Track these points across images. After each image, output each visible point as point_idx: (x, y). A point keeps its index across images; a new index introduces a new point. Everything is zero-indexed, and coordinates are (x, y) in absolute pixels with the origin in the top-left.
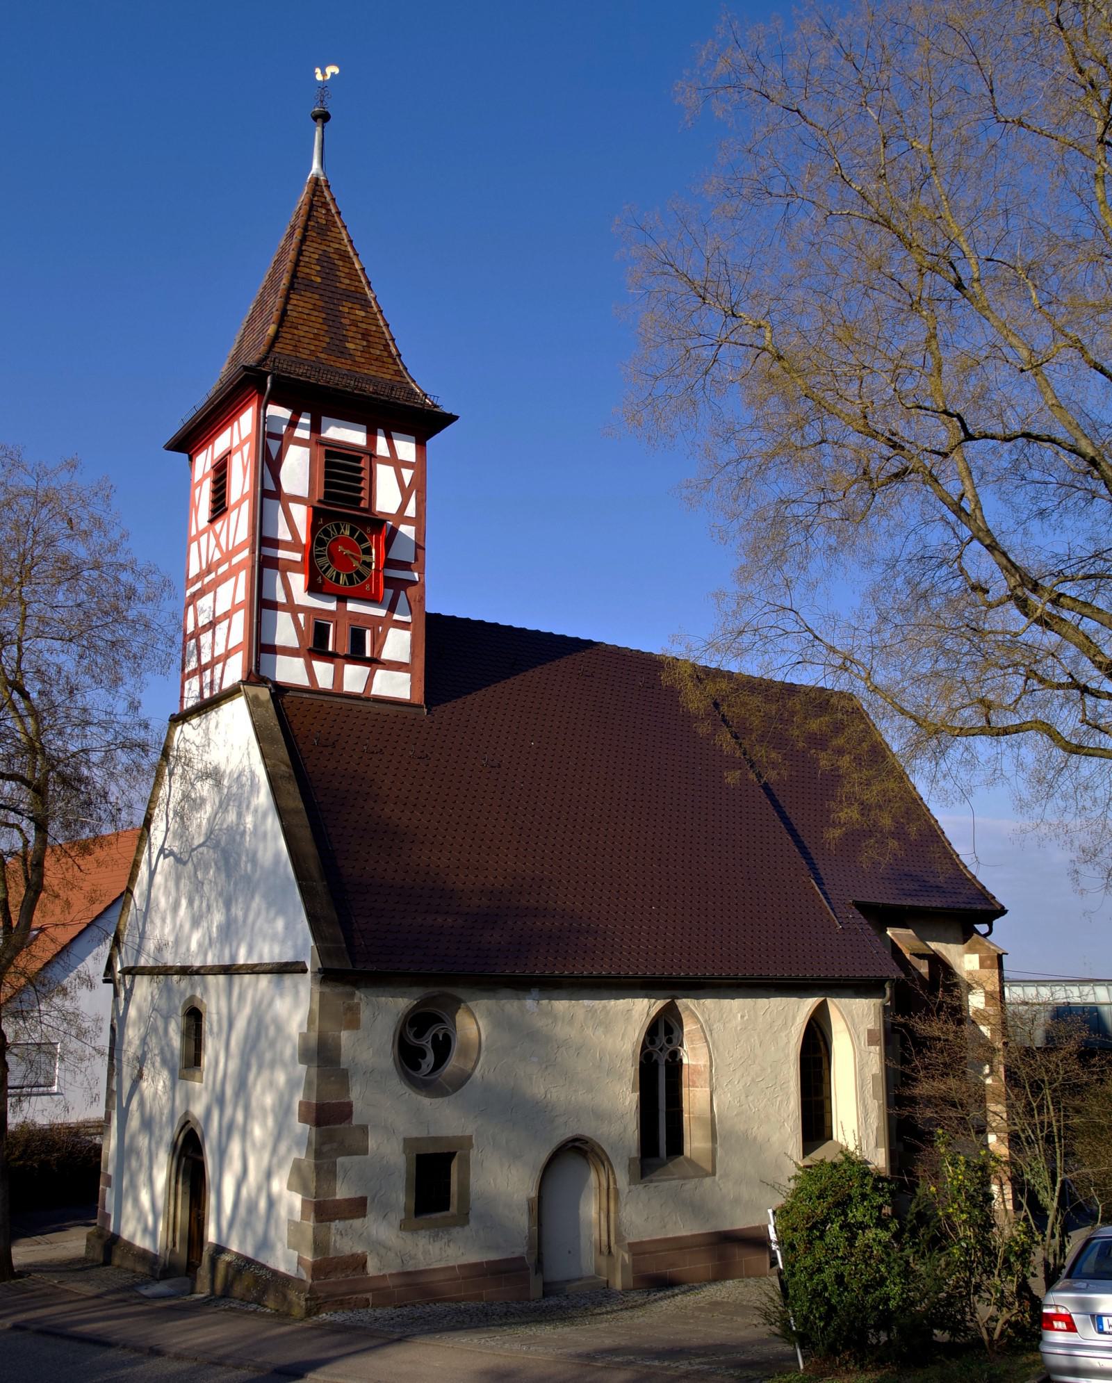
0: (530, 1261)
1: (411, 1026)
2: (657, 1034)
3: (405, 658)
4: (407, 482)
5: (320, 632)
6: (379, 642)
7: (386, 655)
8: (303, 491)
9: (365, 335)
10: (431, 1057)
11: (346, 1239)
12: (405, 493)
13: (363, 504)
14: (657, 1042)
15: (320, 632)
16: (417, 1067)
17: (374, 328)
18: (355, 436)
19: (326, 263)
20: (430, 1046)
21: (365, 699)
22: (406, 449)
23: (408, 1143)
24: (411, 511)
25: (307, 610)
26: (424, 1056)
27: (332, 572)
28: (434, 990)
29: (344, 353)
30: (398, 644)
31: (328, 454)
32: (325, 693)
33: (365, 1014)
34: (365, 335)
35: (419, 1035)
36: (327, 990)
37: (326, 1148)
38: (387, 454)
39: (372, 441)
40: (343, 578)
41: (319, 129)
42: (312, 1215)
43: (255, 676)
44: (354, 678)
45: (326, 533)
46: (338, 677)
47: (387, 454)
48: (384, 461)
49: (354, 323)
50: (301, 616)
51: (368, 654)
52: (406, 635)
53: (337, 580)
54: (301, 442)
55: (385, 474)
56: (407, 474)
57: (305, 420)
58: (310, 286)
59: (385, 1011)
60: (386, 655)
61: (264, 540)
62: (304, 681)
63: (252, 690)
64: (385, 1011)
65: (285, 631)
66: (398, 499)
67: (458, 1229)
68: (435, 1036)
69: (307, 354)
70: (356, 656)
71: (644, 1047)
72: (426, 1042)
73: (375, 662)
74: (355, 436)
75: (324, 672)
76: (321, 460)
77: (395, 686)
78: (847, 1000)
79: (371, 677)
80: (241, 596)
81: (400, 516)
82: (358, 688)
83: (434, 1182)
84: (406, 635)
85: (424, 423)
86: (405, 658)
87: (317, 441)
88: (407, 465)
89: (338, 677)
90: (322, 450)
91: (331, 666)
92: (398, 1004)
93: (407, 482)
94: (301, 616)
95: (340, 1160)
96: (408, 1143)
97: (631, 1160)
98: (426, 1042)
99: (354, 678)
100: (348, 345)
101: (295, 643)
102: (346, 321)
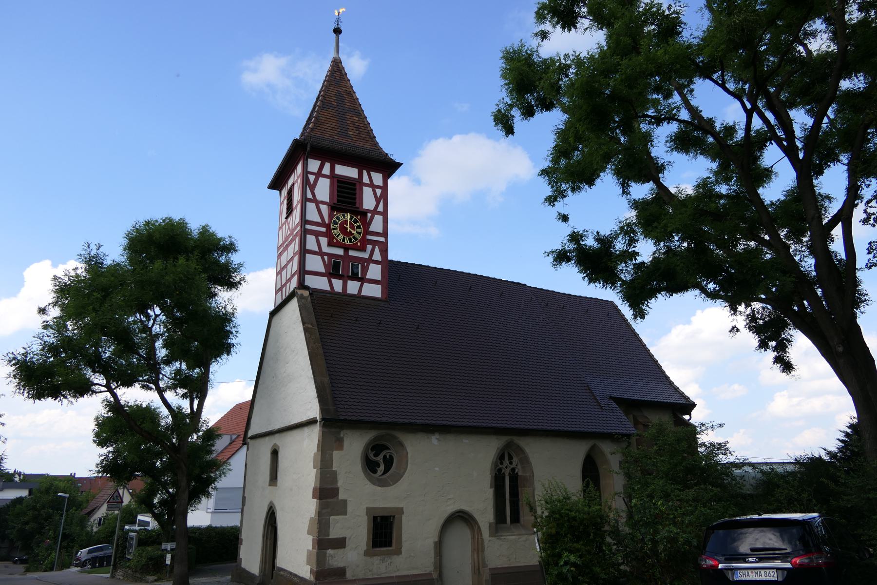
0: (435, 576)
1: (372, 450)
5: (336, 265)
6: (365, 270)
7: (370, 275)
9: (358, 128)
10: (382, 467)
11: (336, 558)
15: (336, 265)
16: (375, 472)
18: (350, 172)
21: (359, 297)
22: (378, 178)
23: (369, 510)
25: (330, 256)
26: (379, 466)
27: (341, 237)
28: (383, 432)
30: (375, 272)
31: (339, 182)
32: (338, 293)
33: (346, 443)
34: (358, 128)
35: (376, 455)
36: (326, 430)
37: (324, 511)
39: (361, 175)
40: (347, 240)
43: (302, 285)
44: (353, 287)
45: (338, 218)
46: (345, 286)
48: (366, 185)
49: (353, 123)
50: (326, 258)
53: (344, 240)
54: (325, 176)
55: (367, 192)
56: (379, 192)
57: (327, 166)
59: (355, 445)
61: (304, 221)
62: (328, 288)
63: (300, 292)
64: (355, 445)
65: (315, 263)
66: (374, 203)
67: (395, 556)
68: (385, 457)
69: (329, 136)
70: (354, 277)
71: (496, 466)
72: (380, 459)
73: (363, 280)
74: (350, 172)
75: (338, 285)
76: (336, 184)
77: (373, 291)
78: (366, 524)
79: (361, 286)
80: (297, 248)
82: (355, 292)
83: (383, 530)
87: (333, 176)
89: (345, 286)
90: (336, 180)
91: (341, 282)
94: (326, 258)
95: (332, 518)
97: (490, 524)
98: (380, 459)
99: (353, 287)
101: (323, 270)
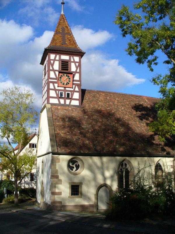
2: (123, 165)
3: (78, 98)
4: (77, 66)
5: (61, 94)
6: (72, 95)
8: (58, 69)
12: (77, 68)
13: (69, 70)
14: (123, 167)
15: (61, 94)
17: (71, 39)
19: (63, 29)
20: (75, 166)
24: (78, 71)
26: (74, 168)
29: (65, 44)
34: (70, 40)
38: (55, 84)
39: (70, 58)
41: (63, 6)
42: (52, 201)
46: (65, 102)
47: (55, 84)
48: (73, 62)
49: (68, 38)
51: (70, 97)
52: (78, 94)
55: (73, 65)
56: (77, 64)
58: (59, 32)
60: (73, 97)
81: (76, 72)
84: (78, 94)
85: (81, 54)
86: (78, 98)
88: (77, 62)
89: (65, 102)
92: (68, 157)
93: (77, 66)
96: (2, 23)
100: (66, 42)
102: (66, 38)
